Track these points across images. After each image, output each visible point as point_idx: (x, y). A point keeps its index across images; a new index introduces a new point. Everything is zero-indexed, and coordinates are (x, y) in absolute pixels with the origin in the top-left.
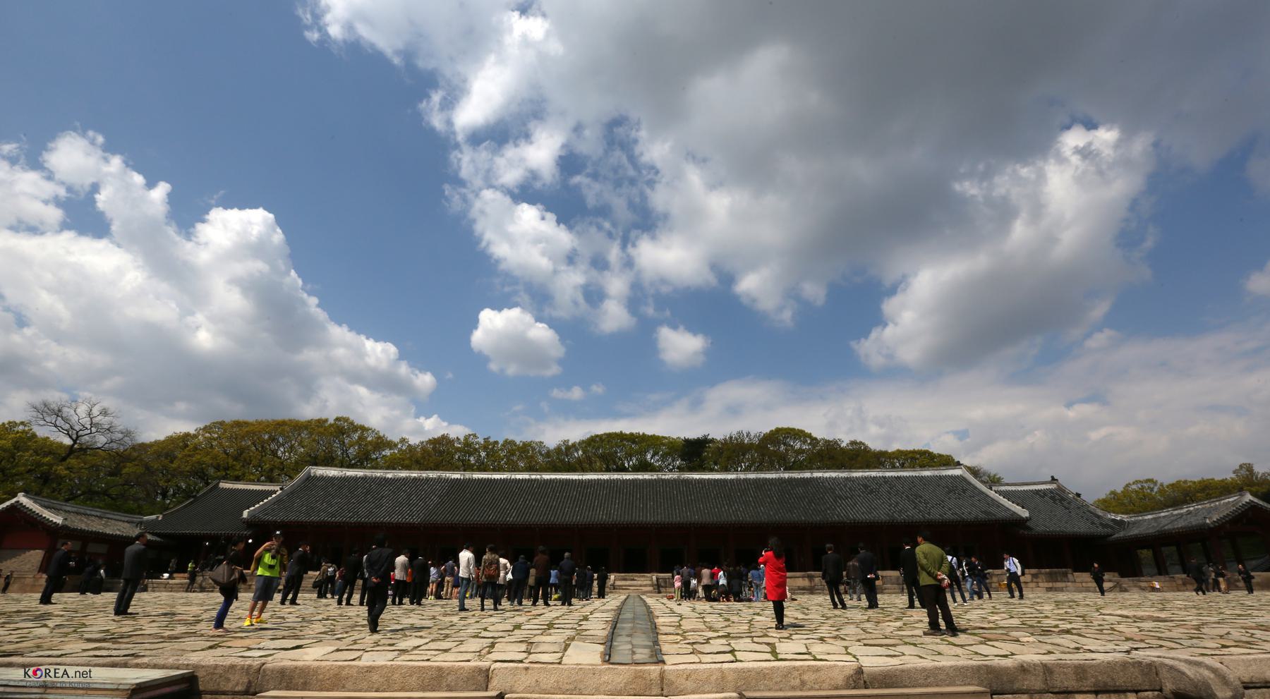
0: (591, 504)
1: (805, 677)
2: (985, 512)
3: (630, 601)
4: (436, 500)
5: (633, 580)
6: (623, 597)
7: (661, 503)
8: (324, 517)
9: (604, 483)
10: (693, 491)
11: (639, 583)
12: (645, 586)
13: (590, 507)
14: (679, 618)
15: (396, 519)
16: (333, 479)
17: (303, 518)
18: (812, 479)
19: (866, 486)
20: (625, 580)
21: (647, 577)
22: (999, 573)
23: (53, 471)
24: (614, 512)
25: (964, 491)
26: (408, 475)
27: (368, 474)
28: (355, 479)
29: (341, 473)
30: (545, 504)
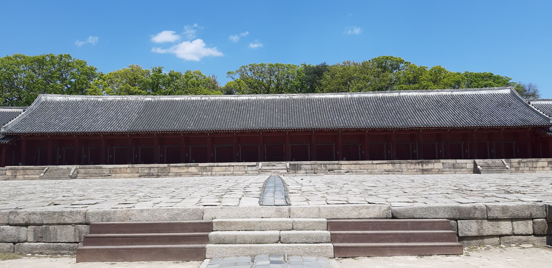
0: (244, 117)
1: (361, 211)
2: (523, 120)
3: (272, 178)
4: (136, 116)
5: (274, 166)
6: (267, 177)
7: (292, 115)
8: (57, 129)
9: (253, 102)
10: (315, 106)
11: (278, 168)
12: (282, 169)
13: (244, 118)
14: (301, 186)
15: (109, 129)
16: (59, 103)
17: (43, 130)
18: (399, 97)
19: (438, 102)
20: (269, 166)
21: (283, 164)
22: (526, 161)
23: (261, 192)
24: (261, 121)
25: (510, 105)
26: (113, 98)
27: (84, 99)
28: (77, 102)
29: (65, 99)
30: (213, 117)
